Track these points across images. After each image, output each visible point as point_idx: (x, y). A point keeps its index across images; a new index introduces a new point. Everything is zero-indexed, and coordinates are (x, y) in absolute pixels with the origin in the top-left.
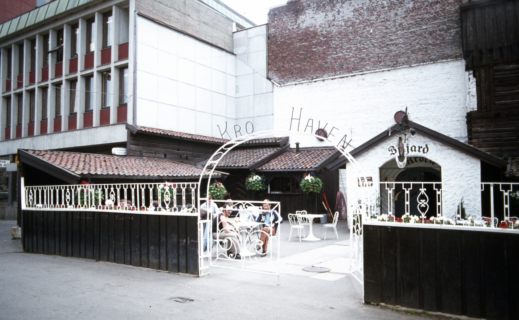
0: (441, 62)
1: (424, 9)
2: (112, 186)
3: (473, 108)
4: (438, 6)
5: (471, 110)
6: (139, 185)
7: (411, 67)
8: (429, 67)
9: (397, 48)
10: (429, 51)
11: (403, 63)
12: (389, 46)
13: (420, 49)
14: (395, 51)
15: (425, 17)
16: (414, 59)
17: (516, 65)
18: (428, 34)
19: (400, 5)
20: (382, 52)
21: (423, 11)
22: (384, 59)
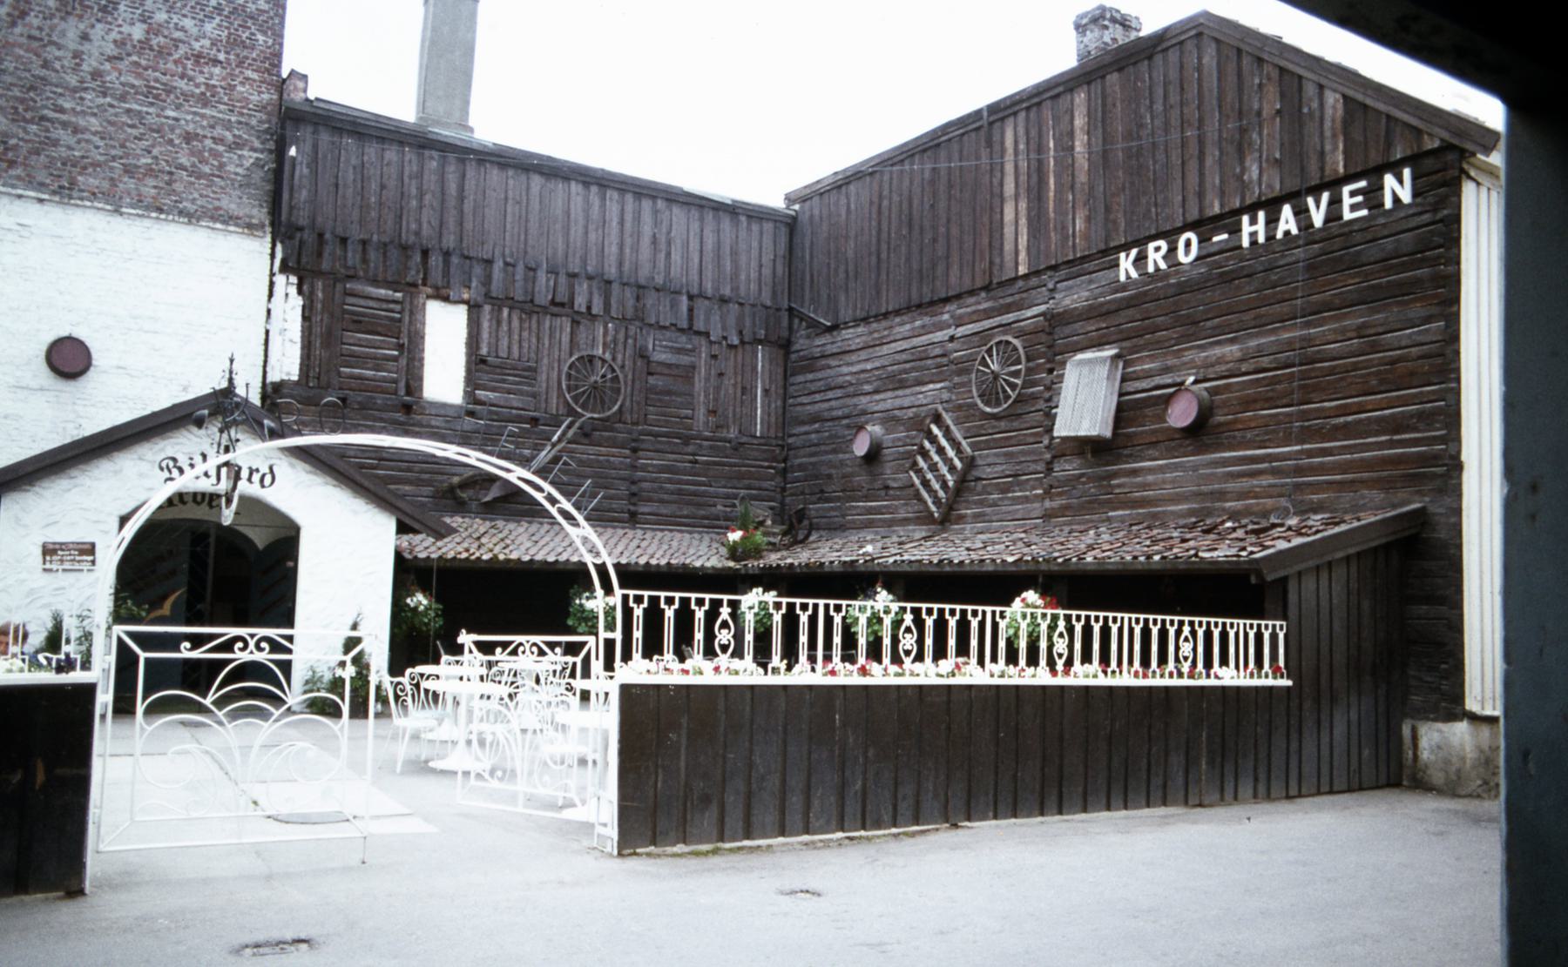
0: (209, 227)
1: (176, 62)
2: (725, 603)
3: (288, 374)
4: (217, 70)
5: (286, 378)
6: (1130, 619)
7: (117, 211)
8: (172, 227)
9: (79, 142)
10: (178, 186)
11: (94, 194)
12: (49, 124)
13: (152, 170)
14: (70, 148)
15: (175, 84)
16: (129, 194)
17: (390, 292)
18: (180, 136)
19: (100, 14)
20: (21, 135)
21: (170, 66)
22: (26, 158)
